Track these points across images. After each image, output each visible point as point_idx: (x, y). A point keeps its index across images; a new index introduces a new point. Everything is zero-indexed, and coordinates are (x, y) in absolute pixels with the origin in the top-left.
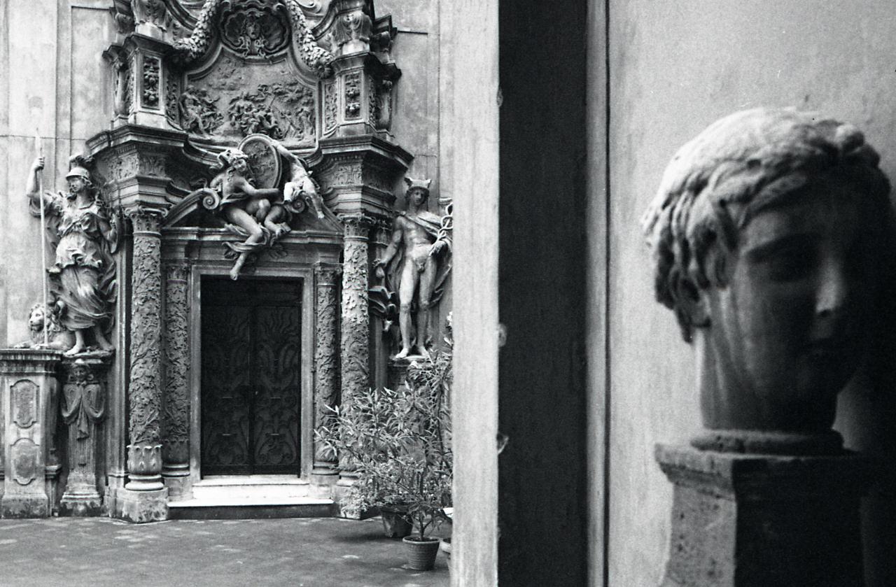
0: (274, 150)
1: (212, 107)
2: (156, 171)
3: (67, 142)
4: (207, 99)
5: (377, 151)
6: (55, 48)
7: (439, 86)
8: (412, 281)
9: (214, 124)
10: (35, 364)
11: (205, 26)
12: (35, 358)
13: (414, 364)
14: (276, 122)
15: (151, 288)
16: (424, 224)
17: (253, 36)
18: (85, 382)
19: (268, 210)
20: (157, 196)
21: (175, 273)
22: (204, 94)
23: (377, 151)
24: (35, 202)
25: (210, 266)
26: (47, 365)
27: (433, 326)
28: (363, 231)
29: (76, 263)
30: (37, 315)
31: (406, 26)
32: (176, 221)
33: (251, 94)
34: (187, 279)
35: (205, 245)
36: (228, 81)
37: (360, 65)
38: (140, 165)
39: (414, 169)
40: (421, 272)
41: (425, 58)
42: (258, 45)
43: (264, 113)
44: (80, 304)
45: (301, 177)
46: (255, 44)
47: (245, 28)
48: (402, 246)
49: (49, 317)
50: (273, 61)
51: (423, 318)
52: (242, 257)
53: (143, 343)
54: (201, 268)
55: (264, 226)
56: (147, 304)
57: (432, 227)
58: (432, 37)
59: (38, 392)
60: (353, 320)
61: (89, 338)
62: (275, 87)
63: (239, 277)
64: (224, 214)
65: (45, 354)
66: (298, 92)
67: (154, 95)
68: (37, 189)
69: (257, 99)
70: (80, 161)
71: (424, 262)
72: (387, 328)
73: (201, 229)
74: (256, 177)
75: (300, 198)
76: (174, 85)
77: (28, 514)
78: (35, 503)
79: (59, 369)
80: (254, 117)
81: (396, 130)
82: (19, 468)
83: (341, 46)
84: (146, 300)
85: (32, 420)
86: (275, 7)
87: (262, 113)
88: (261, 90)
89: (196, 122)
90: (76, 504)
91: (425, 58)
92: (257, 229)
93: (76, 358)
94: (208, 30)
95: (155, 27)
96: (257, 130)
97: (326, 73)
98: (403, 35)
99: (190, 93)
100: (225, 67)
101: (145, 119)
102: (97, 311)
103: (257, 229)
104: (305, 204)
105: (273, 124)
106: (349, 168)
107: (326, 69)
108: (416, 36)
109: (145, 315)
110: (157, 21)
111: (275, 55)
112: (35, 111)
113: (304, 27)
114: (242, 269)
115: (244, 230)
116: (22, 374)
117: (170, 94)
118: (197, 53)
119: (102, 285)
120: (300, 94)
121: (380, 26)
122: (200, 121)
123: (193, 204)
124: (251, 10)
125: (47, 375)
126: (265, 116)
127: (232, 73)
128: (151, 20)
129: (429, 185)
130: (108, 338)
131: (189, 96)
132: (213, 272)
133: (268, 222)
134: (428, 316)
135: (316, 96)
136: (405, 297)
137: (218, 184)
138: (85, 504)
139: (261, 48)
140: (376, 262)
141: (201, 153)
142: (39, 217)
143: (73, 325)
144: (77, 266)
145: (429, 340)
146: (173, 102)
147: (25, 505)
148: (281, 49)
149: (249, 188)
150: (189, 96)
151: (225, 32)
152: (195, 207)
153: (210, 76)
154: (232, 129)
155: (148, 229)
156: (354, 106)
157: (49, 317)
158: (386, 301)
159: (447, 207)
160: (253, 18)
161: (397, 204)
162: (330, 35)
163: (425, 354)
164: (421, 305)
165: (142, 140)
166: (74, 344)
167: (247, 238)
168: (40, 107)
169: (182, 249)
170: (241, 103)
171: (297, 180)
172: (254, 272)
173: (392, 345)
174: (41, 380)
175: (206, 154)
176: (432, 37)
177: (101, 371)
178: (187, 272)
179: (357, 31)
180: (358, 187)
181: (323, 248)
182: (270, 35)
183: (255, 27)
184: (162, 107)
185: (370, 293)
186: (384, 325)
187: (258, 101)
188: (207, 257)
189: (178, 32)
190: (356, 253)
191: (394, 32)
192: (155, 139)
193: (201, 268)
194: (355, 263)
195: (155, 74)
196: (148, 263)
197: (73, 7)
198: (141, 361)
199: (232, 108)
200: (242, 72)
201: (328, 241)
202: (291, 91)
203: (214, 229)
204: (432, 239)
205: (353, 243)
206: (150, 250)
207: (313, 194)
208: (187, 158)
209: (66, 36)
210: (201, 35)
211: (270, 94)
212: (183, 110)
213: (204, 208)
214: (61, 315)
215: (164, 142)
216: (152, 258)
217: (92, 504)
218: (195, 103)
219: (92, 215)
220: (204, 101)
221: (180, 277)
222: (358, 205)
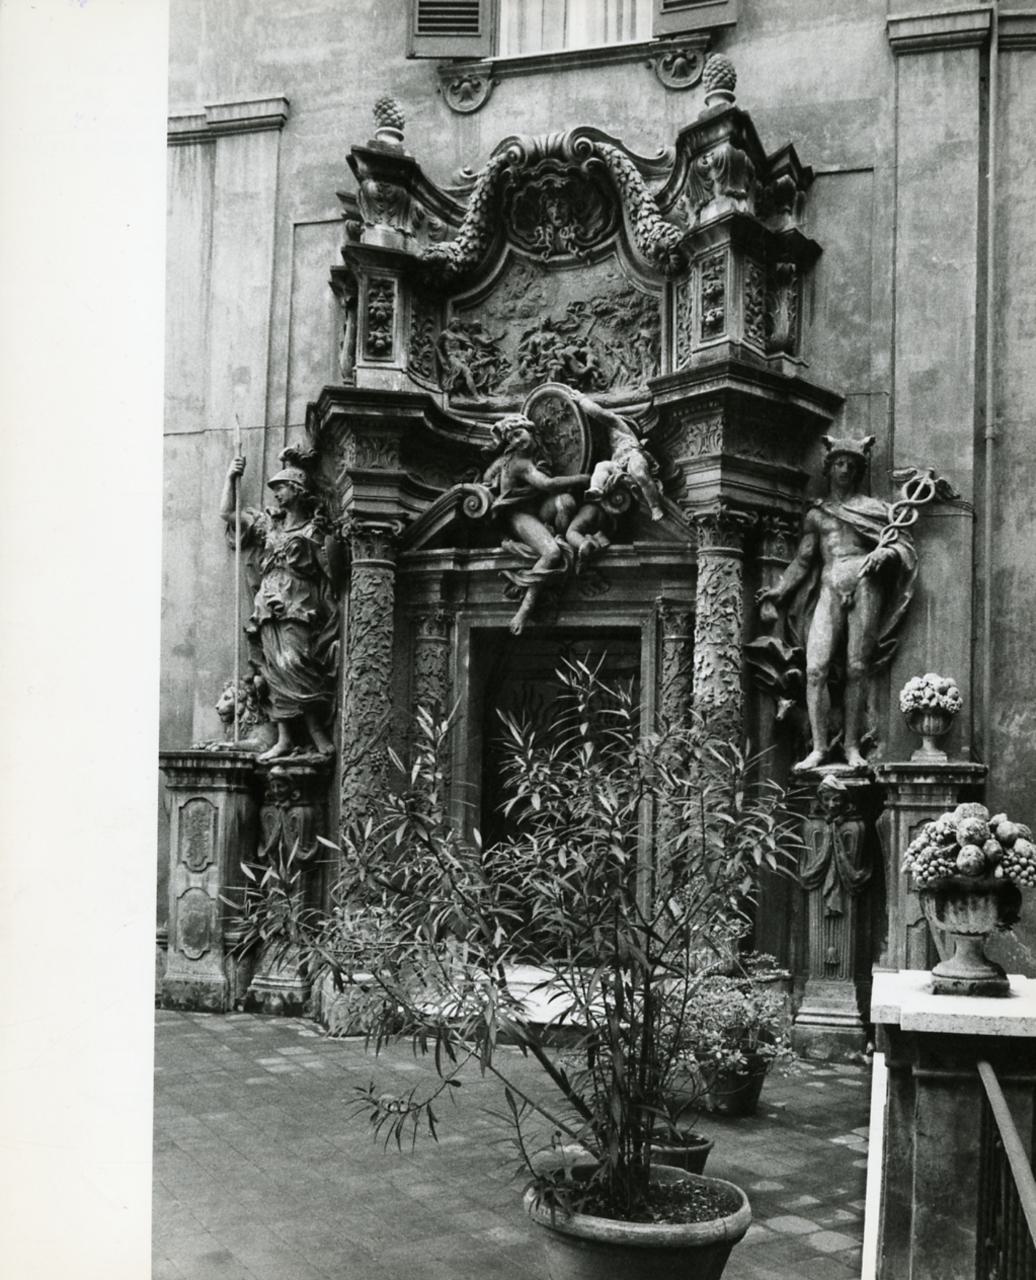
0: (575, 407)
1: (491, 349)
2: (386, 460)
3: (281, 431)
4: (483, 338)
5: (746, 389)
6: (269, 290)
7: (894, 263)
8: (830, 627)
9: (495, 377)
10: (212, 773)
11: (476, 218)
12: (211, 765)
13: (829, 780)
14: (594, 362)
15: (371, 652)
16: (852, 518)
17: (557, 223)
18: (286, 804)
19: (572, 513)
20: (385, 502)
21: (426, 625)
22: (478, 329)
23: (746, 389)
24: (230, 527)
25: (485, 613)
26: (229, 775)
27: (877, 707)
28: (729, 537)
29: (274, 616)
30: (226, 698)
31: (832, 163)
32: (424, 541)
33: (554, 320)
34: (448, 635)
35: (475, 577)
36: (520, 304)
37: (724, 239)
38: (358, 453)
39: (844, 421)
40: (848, 608)
41: (868, 216)
42: (567, 235)
43: (574, 349)
44: (283, 681)
45: (626, 450)
46: (562, 236)
47: (545, 209)
48: (817, 562)
49: (243, 700)
50: (592, 259)
51: (853, 695)
52: (529, 595)
53: (358, 741)
54: (471, 617)
55: (564, 539)
56: (365, 678)
57: (869, 524)
58: (883, 172)
59: (216, 816)
60: (707, 699)
61: (298, 734)
62: (597, 302)
63: (525, 629)
64: (500, 525)
65: (224, 758)
66: (634, 305)
67: (384, 339)
68: (232, 508)
69: (565, 327)
70: (291, 458)
71: (852, 587)
72: (780, 714)
73: (460, 551)
74: (554, 457)
75: (619, 486)
76: (430, 321)
77: (196, 1004)
78: (207, 988)
79: (249, 780)
80: (555, 357)
81: (811, 351)
82: (188, 932)
83: (698, 213)
84: (363, 671)
85: (207, 860)
86: (584, 166)
87: (571, 350)
88: (573, 311)
89: (461, 376)
90: (267, 995)
91: (868, 216)
92: (549, 545)
93: (272, 765)
94: (483, 224)
95: (392, 229)
96: (562, 376)
97: (674, 264)
98: (826, 180)
99: (455, 331)
100: (516, 281)
101: (368, 378)
102: (305, 691)
103: (549, 545)
104: (632, 498)
105: (590, 364)
106: (703, 426)
107: (672, 257)
108: (851, 176)
109: (360, 695)
110: (394, 221)
111: (595, 249)
112: (240, 389)
113: (639, 193)
114: (530, 615)
115: (529, 549)
116: (194, 789)
117: (420, 335)
118: (463, 263)
119: (317, 648)
120: (637, 310)
121: (775, 169)
122: (468, 373)
123: (450, 510)
124: (545, 179)
125: (229, 791)
126: (576, 354)
127: (526, 289)
128: (385, 220)
129: (867, 447)
130: (329, 733)
131: (450, 335)
132: (490, 623)
133: (573, 535)
134: (865, 691)
135: (662, 309)
136: (816, 659)
137: (493, 477)
138: (281, 996)
139: (569, 240)
140: (760, 594)
141: (466, 426)
142: (234, 549)
143: (276, 714)
144: (276, 619)
145: (868, 735)
146: (426, 348)
147: (194, 990)
148: (604, 239)
149: (536, 476)
150: (450, 335)
151: (511, 223)
152: (451, 516)
153: (492, 299)
154: (522, 382)
155: (370, 556)
156: (712, 314)
157: (243, 700)
158: (781, 665)
159: (906, 485)
160: (552, 192)
161: (810, 487)
162: (684, 198)
163: (855, 760)
164: (849, 670)
165: (351, 411)
166: (276, 741)
167: (536, 561)
168: (247, 383)
169: (437, 587)
170: (538, 338)
171: (620, 456)
172: (556, 619)
173: (796, 746)
174: (220, 799)
175: (474, 427)
176: (883, 172)
177: (318, 786)
178: (446, 625)
179: (722, 180)
180: (714, 458)
181: (669, 572)
182: (589, 216)
183: (559, 207)
184: (400, 357)
185: (747, 652)
186: (777, 707)
187: (568, 331)
188: (479, 598)
189: (439, 234)
190: (714, 578)
191: (807, 178)
192: (373, 408)
193: (471, 617)
194: (713, 595)
195: (387, 304)
196: (368, 611)
197: (296, 225)
198: (354, 770)
199: (525, 348)
200: (544, 286)
201: (673, 560)
202: (622, 306)
203: (482, 551)
204: (868, 545)
205: (709, 559)
206: (371, 589)
207: (640, 479)
208: (442, 437)
209: (285, 269)
210: (469, 234)
211: (588, 317)
212: (443, 360)
213: (466, 516)
214: (260, 697)
215: (389, 411)
216: (375, 603)
217: (291, 996)
218: (463, 346)
219: (302, 541)
220: (477, 342)
221: (435, 631)
222: (717, 491)
